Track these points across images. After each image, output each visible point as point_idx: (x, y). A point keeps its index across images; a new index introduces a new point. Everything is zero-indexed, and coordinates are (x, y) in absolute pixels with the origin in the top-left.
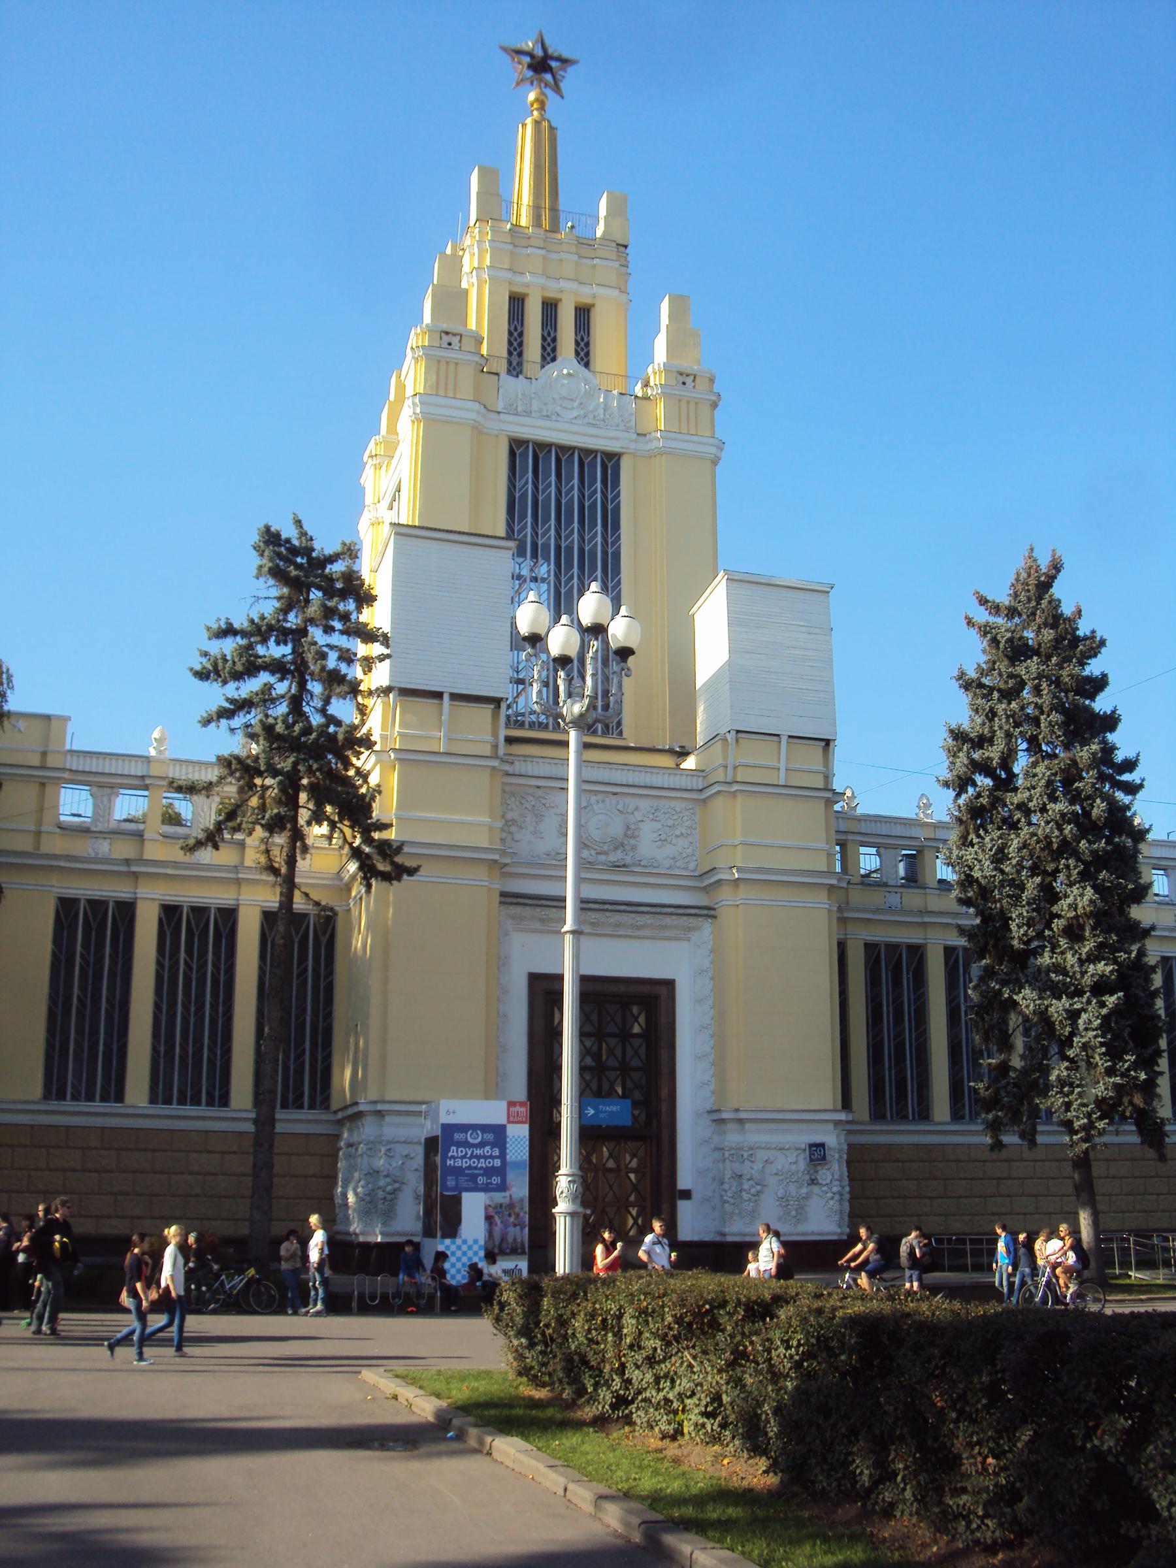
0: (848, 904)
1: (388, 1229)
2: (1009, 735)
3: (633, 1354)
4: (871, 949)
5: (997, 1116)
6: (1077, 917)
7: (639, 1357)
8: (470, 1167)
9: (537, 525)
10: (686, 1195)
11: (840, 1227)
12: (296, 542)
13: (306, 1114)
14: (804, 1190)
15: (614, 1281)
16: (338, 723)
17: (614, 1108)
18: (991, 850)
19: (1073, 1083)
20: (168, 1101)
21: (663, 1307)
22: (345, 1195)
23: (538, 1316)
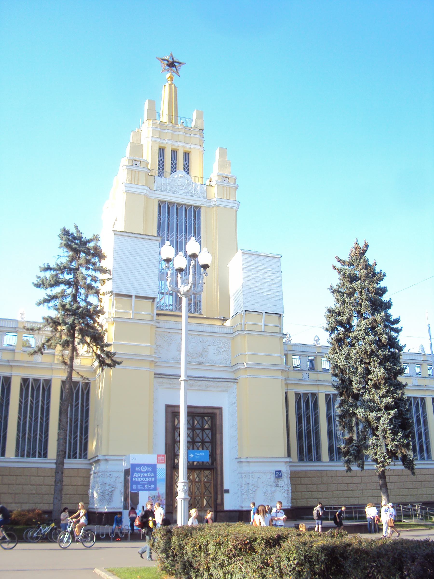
0: (288, 378)
1: (110, 506)
2: (350, 310)
3: (213, 562)
4: (297, 394)
5: (349, 458)
6: (378, 380)
7: (217, 563)
8: (142, 481)
9: (169, 233)
10: (227, 491)
11: (288, 503)
12: (75, 235)
13: (78, 461)
14: (274, 489)
15: (204, 529)
16: (91, 305)
17: (202, 454)
18: (344, 354)
19: (378, 445)
20: (23, 456)
21: (228, 541)
22: (92, 493)
23: (170, 544)
